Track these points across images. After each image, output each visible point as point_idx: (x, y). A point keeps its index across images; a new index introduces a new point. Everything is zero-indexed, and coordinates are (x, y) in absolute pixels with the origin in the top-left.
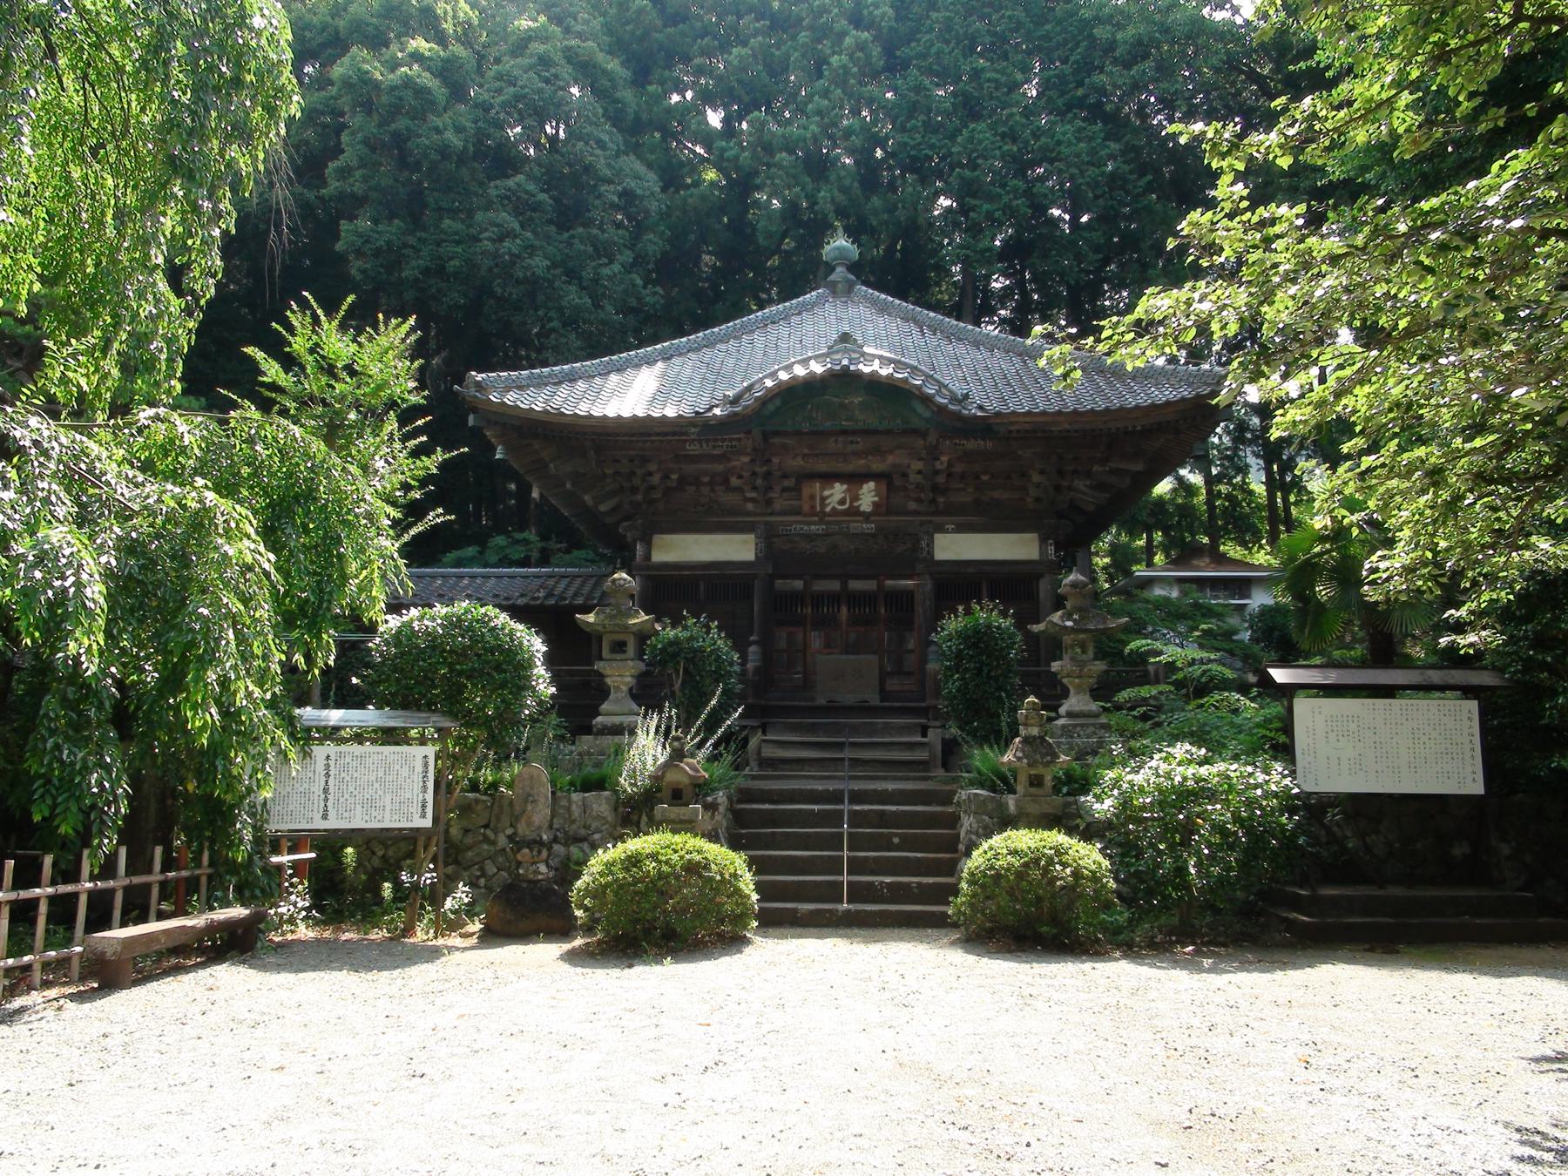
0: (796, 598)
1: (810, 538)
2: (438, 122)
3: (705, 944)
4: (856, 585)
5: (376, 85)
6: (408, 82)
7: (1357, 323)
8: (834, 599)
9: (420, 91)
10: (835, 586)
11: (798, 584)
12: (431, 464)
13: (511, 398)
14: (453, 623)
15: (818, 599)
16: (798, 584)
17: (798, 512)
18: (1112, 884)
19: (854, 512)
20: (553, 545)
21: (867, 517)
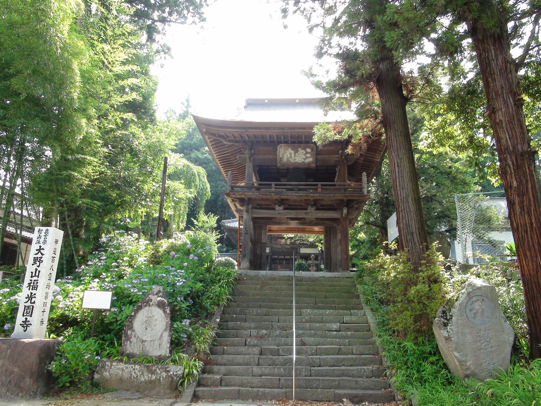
0: (276, 259)
1: (279, 248)
2: (211, 165)
3: (63, 389)
4: (286, 257)
5: (200, 158)
6: (206, 158)
7: (495, 181)
8: (283, 259)
9: (208, 159)
10: (283, 257)
11: (276, 257)
12: (219, 237)
13: (229, 225)
14: (226, 260)
15: (280, 259)
16: (276, 257)
17: (276, 244)
18: (458, 124)
19: (286, 244)
20: (229, 248)
21: (289, 245)
